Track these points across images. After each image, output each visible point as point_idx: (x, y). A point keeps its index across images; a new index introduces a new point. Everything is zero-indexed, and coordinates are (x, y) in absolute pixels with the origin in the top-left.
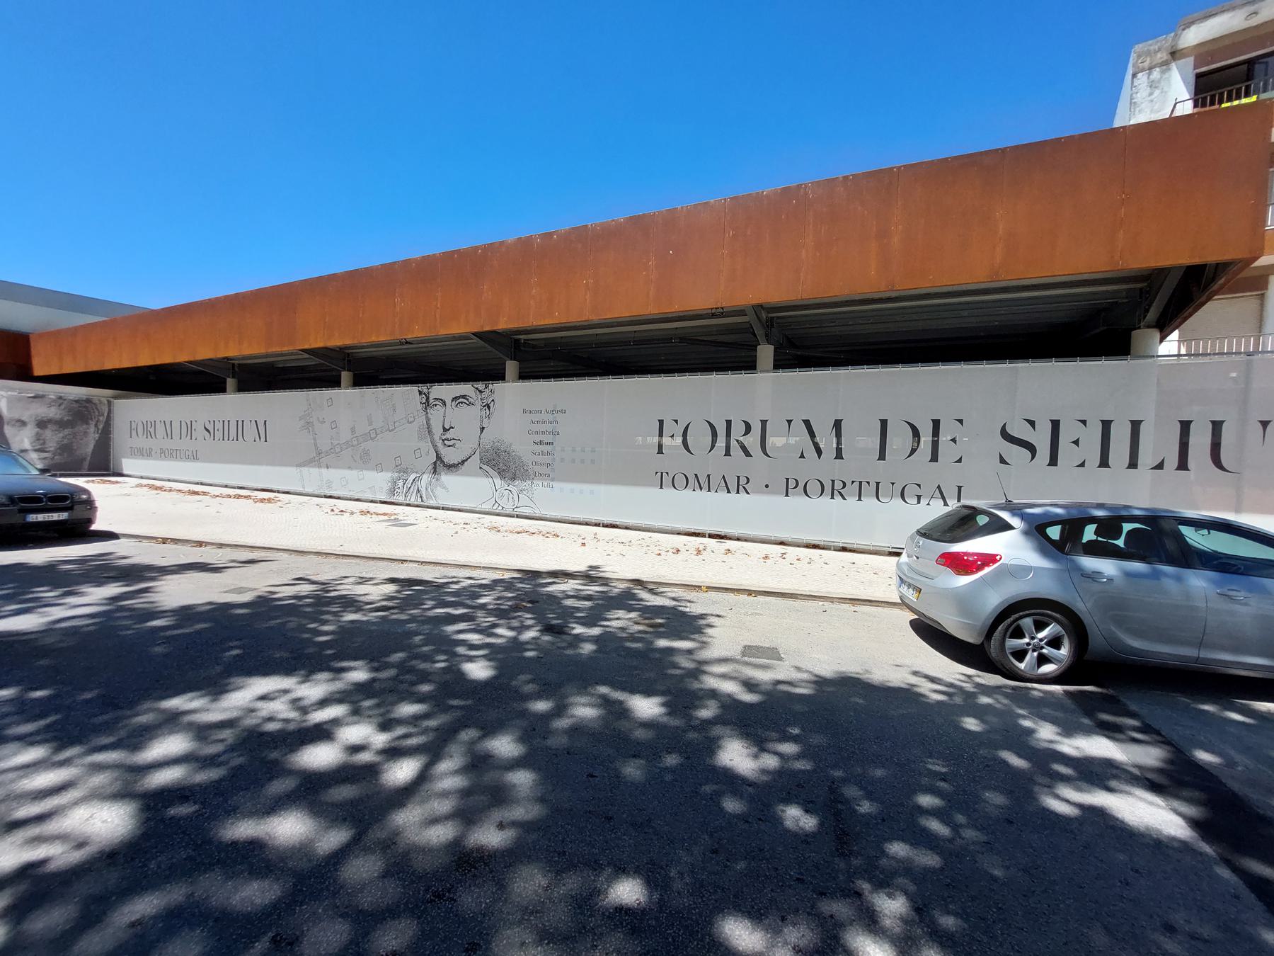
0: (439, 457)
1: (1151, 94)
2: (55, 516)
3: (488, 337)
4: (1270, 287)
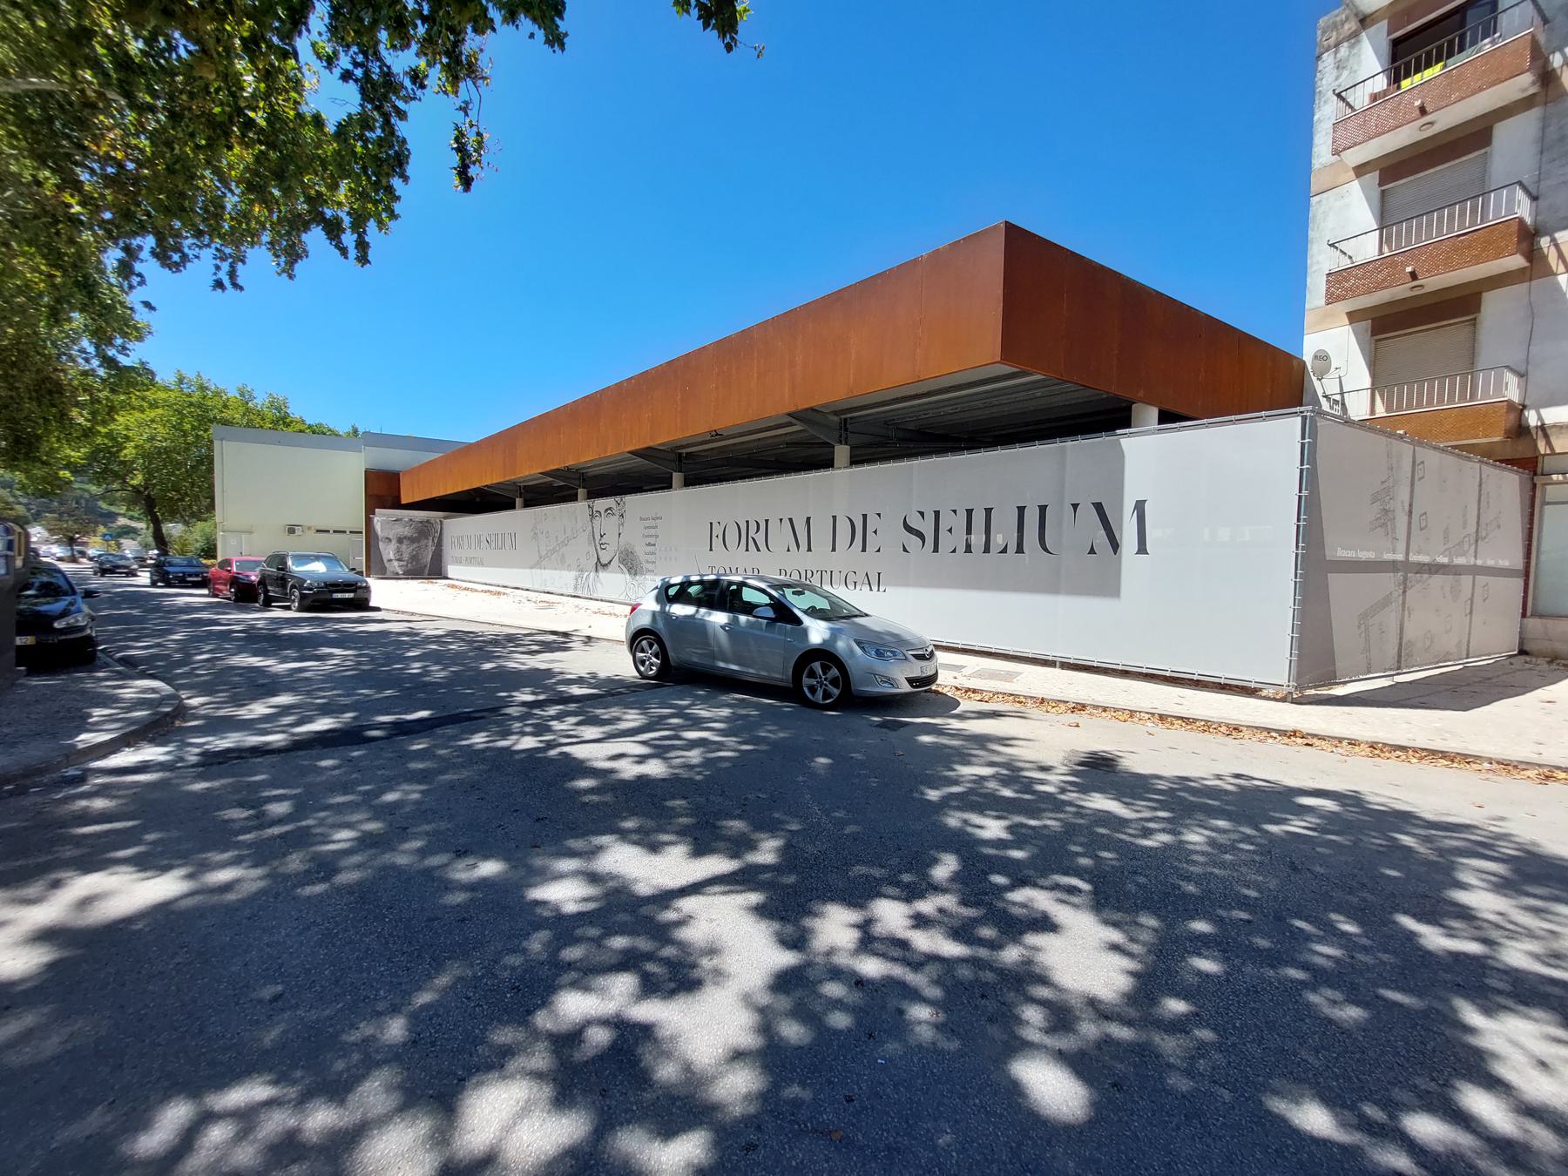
1: (1337, 78)
2: (347, 595)
3: (646, 453)
4: (1482, 309)
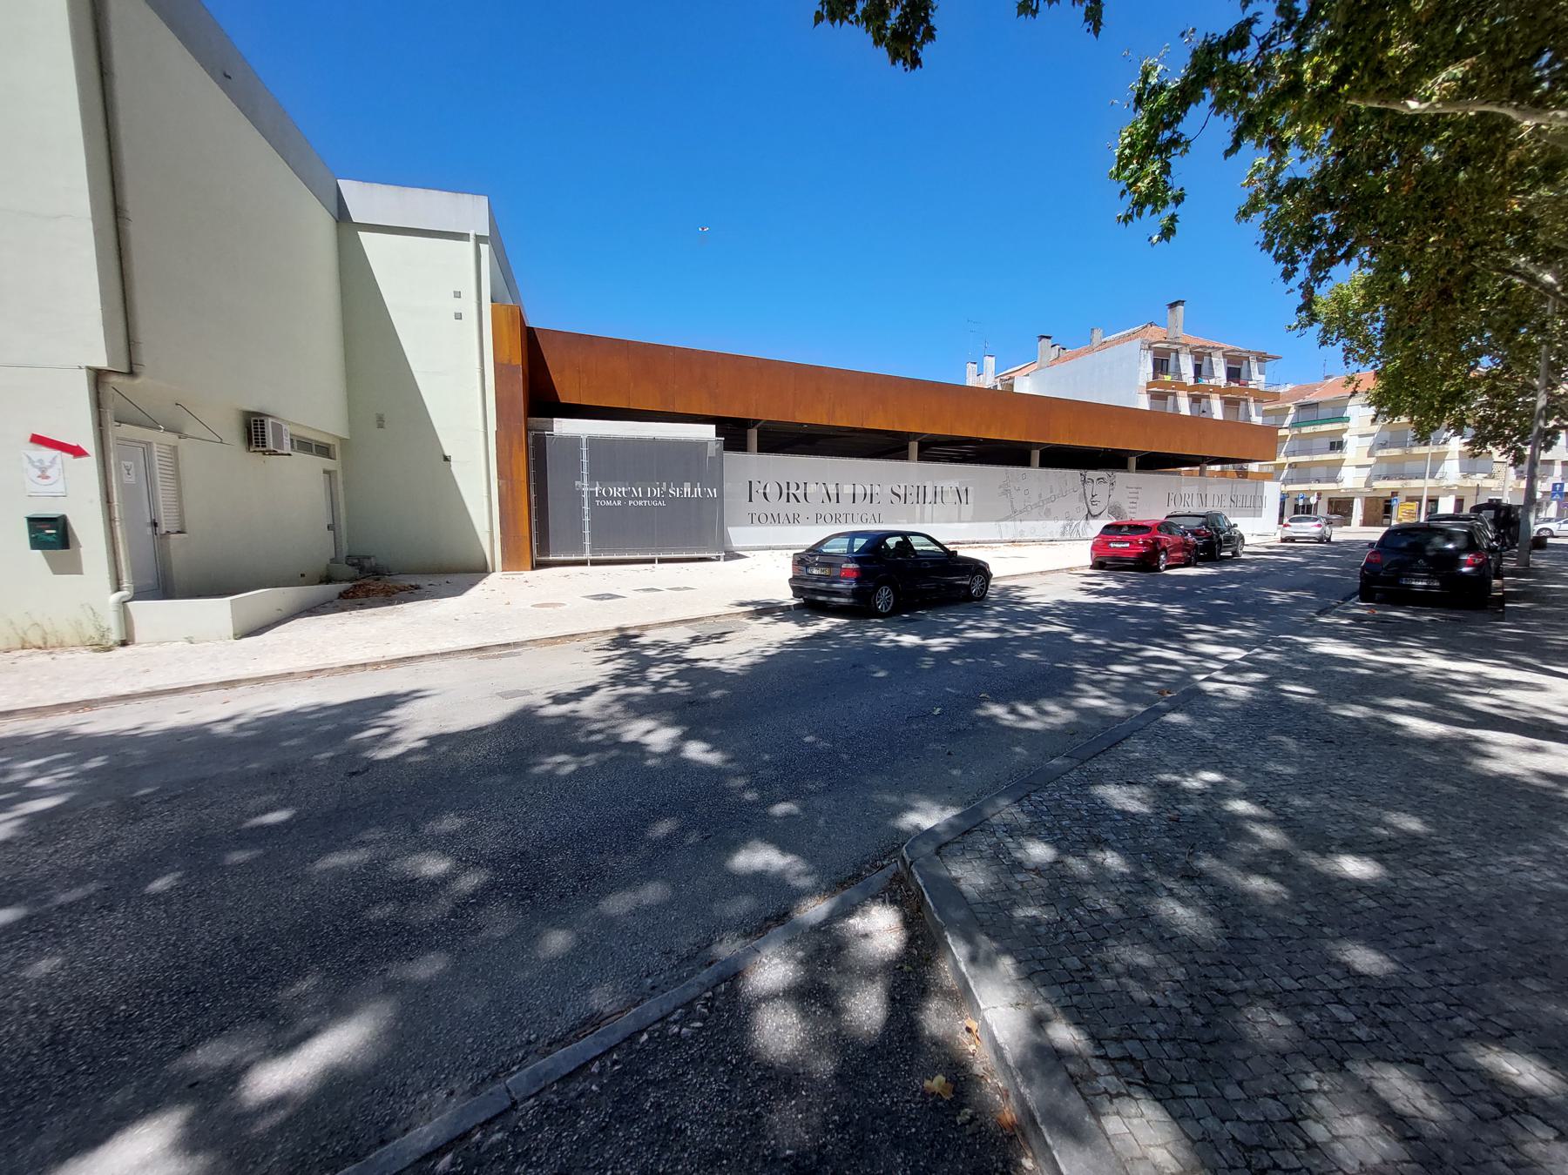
0: (1089, 512)
